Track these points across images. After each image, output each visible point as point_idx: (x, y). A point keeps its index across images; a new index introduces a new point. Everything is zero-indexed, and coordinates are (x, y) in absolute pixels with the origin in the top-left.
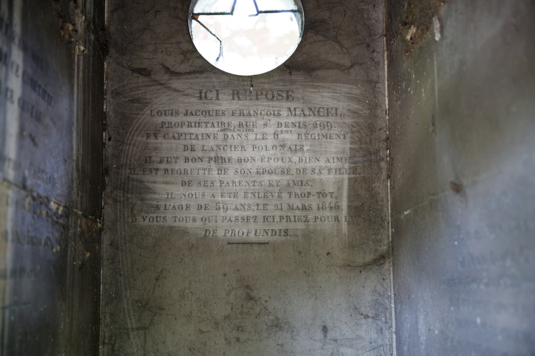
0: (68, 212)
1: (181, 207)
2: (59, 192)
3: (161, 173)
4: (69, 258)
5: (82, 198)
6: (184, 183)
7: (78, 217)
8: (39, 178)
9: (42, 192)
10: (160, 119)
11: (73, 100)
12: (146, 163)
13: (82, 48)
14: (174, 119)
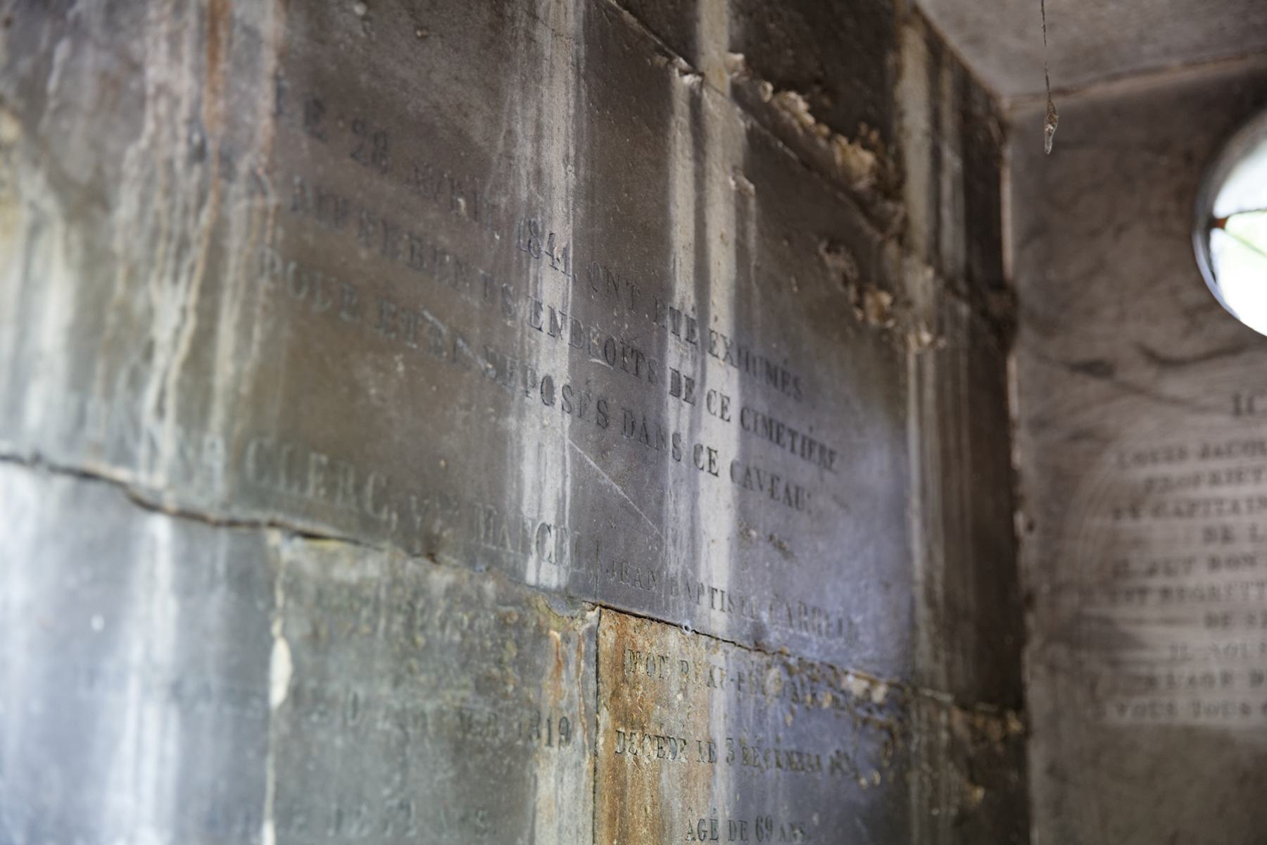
0: (904, 696)
1: (1208, 679)
2: (869, 653)
3: (1153, 599)
4: (914, 800)
5: (950, 665)
6: (1211, 621)
7: (939, 706)
8: (804, 625)
9: (811, 654)
10: (1142, 474)
11: (906, 451)
12: (1116, 577)
13: (926, 338)
14: (1175, 470)
